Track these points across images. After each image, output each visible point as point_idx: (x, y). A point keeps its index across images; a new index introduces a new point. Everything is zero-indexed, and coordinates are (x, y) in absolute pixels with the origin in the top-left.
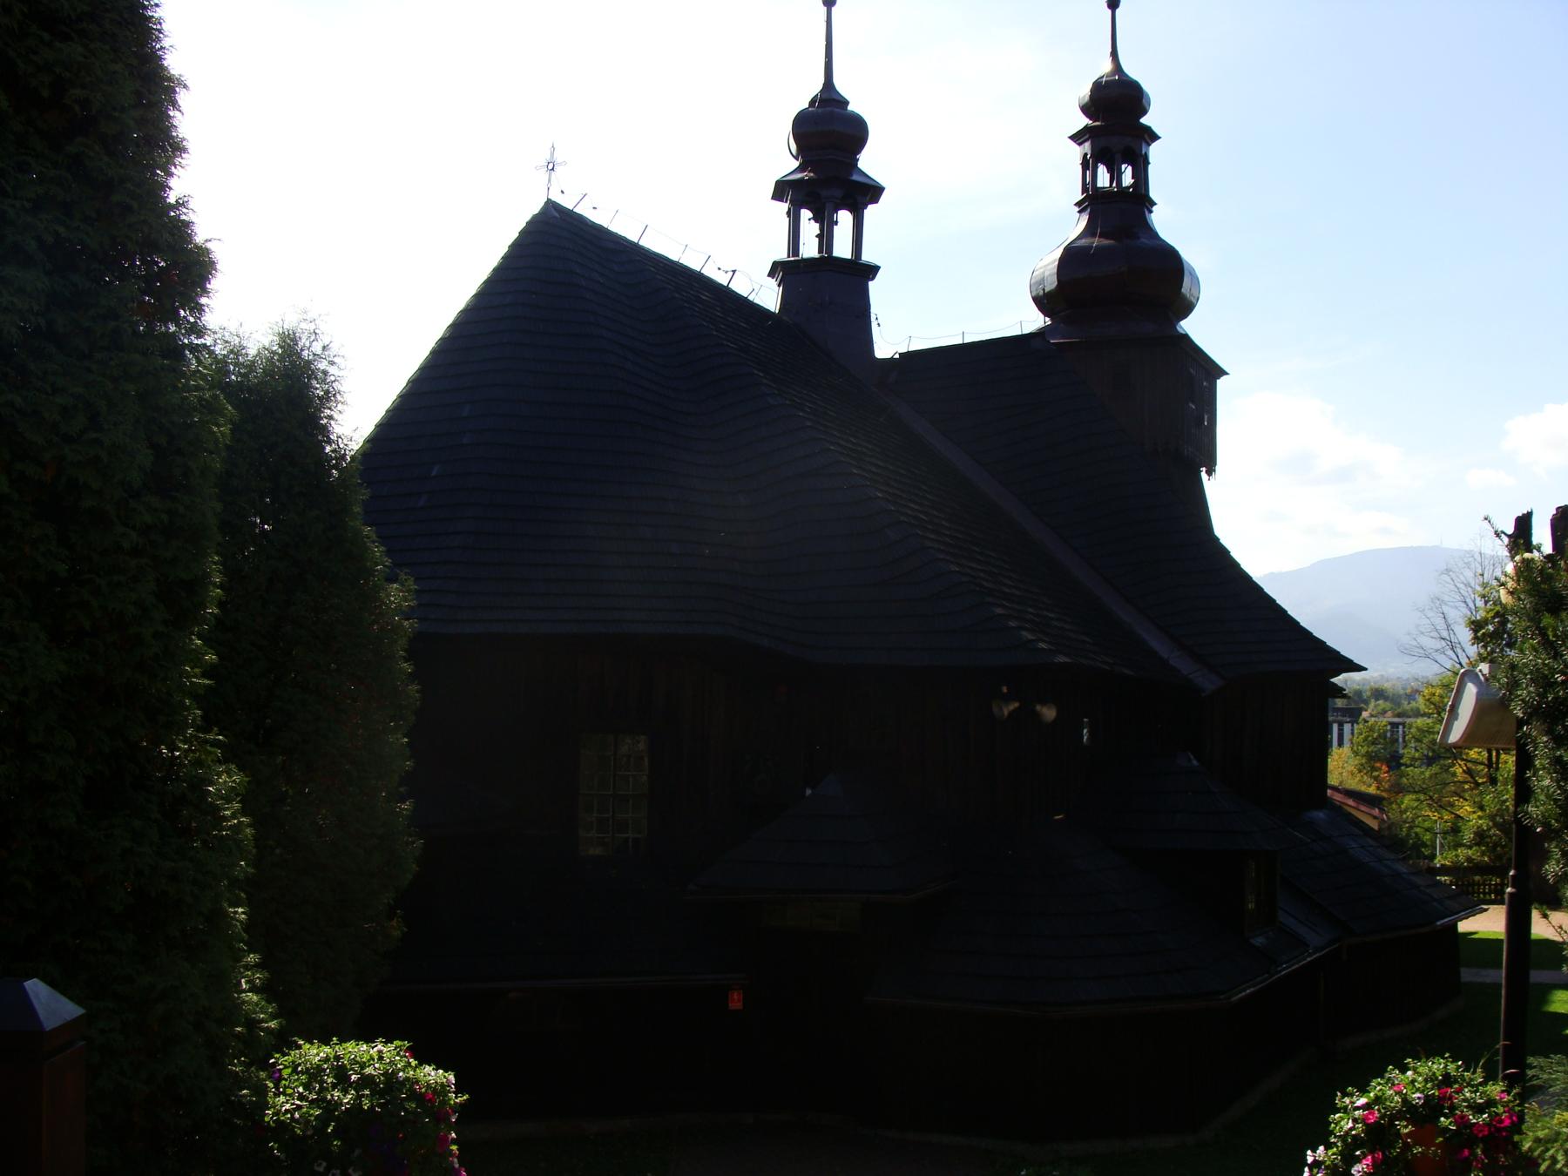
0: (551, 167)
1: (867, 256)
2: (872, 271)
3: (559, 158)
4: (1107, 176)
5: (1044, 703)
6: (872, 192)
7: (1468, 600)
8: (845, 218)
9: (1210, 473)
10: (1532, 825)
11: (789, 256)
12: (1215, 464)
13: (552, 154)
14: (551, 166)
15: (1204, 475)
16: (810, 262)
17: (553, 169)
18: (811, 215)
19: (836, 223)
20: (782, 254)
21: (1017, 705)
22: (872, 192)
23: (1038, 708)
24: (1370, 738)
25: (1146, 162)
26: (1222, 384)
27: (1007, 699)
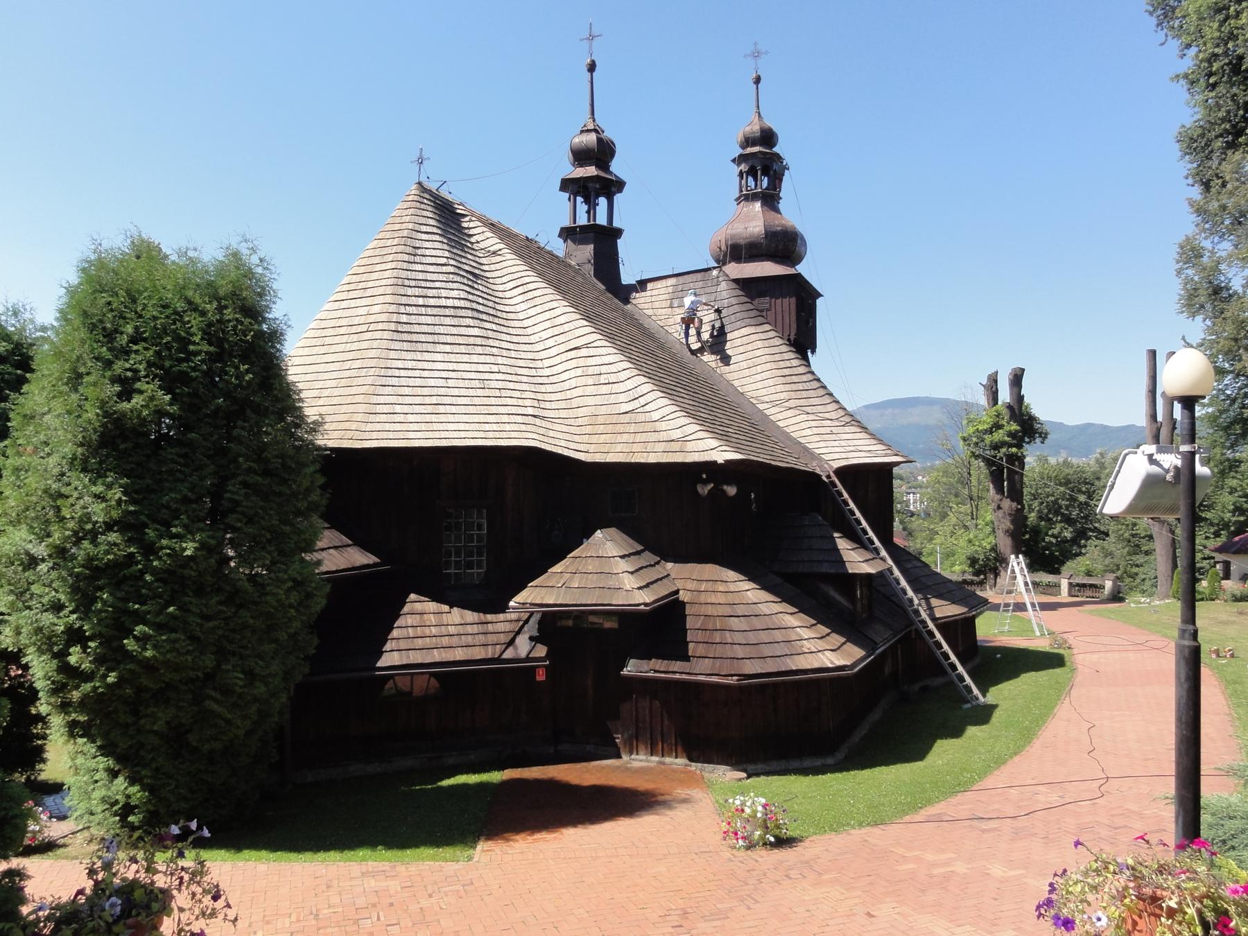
1: (616, 224)
3: (425, 155)
4: (753, 183)
5: (729, 484)
6: (619, 185)
7: (958, 423)
8: (603, 201)
10: (78, 707)
13: (421, 153)
14: (420, 161)
16: (582, 227)
17: (421, 163)
18: (582, 200)
19: (598, 204)
20: (567, 222)
21: (712, 485)
22: (619, 185)
23: (725, 487)
24: (982, 476)
26: (820, 302)
27: (705, 482)
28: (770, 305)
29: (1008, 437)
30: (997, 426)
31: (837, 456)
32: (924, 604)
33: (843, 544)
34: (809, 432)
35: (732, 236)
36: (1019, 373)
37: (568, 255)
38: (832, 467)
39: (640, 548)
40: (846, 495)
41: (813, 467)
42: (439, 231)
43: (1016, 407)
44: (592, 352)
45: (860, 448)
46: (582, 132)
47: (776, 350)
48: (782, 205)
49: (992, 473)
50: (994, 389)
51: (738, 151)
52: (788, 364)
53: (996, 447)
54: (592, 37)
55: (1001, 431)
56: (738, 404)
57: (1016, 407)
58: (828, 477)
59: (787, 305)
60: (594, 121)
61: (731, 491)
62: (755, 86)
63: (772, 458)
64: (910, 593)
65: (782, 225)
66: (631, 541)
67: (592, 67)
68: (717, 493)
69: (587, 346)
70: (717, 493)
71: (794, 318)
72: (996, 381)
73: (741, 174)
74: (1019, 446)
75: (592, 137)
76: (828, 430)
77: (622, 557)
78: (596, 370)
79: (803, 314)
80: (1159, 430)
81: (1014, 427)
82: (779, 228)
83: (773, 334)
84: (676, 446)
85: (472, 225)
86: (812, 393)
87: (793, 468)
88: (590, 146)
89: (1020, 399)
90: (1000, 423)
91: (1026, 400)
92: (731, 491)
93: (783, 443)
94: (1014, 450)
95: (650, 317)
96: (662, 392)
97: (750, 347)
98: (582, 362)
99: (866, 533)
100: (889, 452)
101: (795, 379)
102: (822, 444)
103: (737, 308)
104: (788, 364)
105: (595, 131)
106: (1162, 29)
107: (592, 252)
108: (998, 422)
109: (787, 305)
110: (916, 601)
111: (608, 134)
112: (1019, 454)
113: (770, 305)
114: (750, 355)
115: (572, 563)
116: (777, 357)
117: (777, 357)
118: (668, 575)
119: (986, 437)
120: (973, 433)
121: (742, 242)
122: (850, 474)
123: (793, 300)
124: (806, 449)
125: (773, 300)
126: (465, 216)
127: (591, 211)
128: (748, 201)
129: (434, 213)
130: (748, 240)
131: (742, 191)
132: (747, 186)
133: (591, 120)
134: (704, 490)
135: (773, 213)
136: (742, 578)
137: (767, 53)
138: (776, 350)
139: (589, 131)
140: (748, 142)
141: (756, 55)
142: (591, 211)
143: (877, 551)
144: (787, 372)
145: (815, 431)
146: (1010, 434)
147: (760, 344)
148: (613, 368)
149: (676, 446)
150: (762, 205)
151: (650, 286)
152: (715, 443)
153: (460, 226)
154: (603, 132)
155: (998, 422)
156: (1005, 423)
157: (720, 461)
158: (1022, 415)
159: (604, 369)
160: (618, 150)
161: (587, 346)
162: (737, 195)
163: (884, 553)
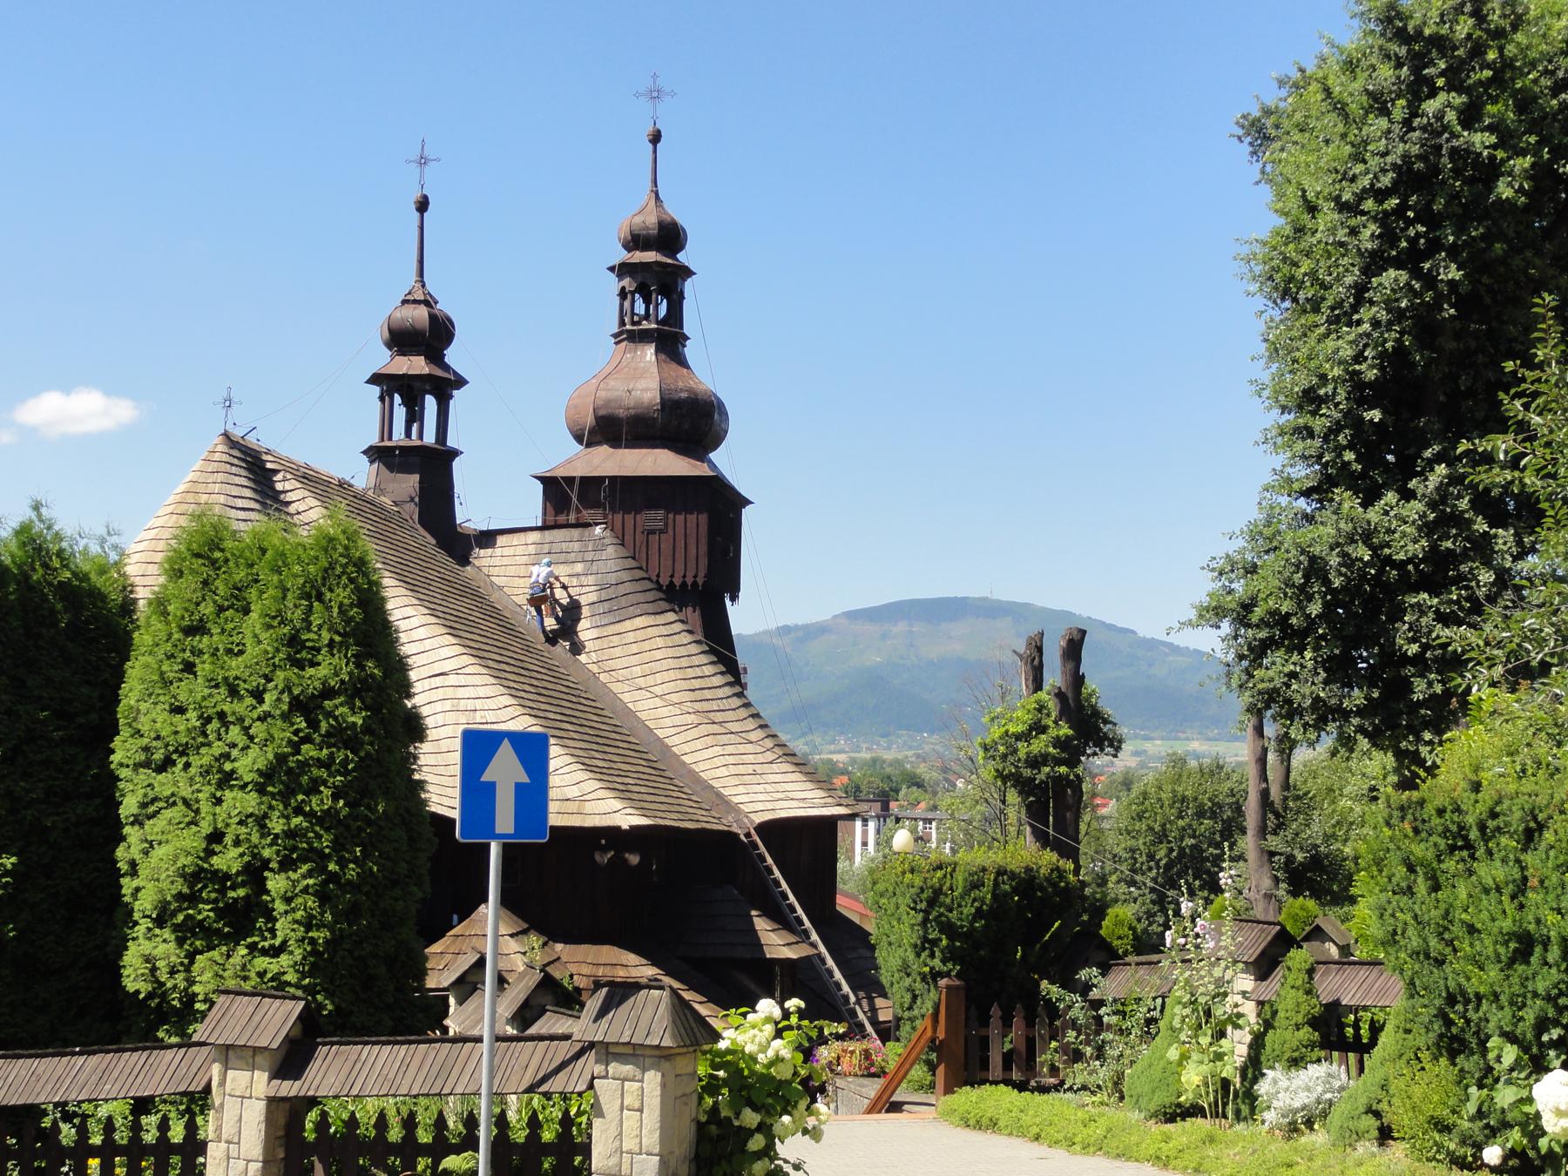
0: (228, 403)
1: (451, 442)
2: (454, 453)
5: (631, 851)
9: (734, 598)
11: (383, 440)
12: (738, 590)
14: (227, 403)
15: (728, 602)
20: (373, 439)
25: (681, 296)
26: (746, 513)
27: (604, 849)
28: (666, 525)
29: (1055, 748)
30: (1038, 728)
31: (760, 806)
32: (865, 1003)
33: (761, 924)
34: (724, 771)
35: (608, 402)
36: (1076, 637)
37: (379, 489)
38: (752, 821)
39: (526, 926)
40: (770, 860)
41: (726, 823)
42: (257, 506)
43: (1070, 695)
44: (462, 680)
45: (791, 795)
46: (404, 302)
47: (682, 651)
48: (690, 351)
49: (1029, 807)
50: (1036, 662)
51: (621, 255)
52: (698, 672)
53: (1035, 762)
54: (423, 161)
55: (1043, 737)
56: (630, 729)
57: (1070, 695)
58: (748, 835)
59: (693, 524)
60: (423, 286)
61: (634, 859)
62: (650, 146)
63: (680, 816)
64: (846, 988)
65: (690, 390)
66: (520, 921)
67: (423, 205)
68: (618, 862)
69: (456, 672)
70: (618, 862)
71: (703, 548)
72: (1040, 649)
73: (623, 294)
74: (1073, 762)
75: (422, 313)
76: (750, 769)
77: (512, 936)
78: (470, 704)
79: (719, 539)
80: (1265, 750)
81: (1065, 730)
82: (684, 395)
83: (678, 627)
84: (572, 807)
85: (288, 486)
86: (730, 715)
87: (703, 830)
88: (418, 326)
89: (1078, 680)
90: (1043, 723)
91: (1091, 684)
92: (634, 859)
93: (690, 788)
94: (1063, 769)
95: (501, 588)
96: (535, 716)
97: (646, 646)
98: (450, 692)
99: (793, 910)
100: (830, 800)
101: (707, 694)
102: (741, 789)
103: (628, 587)
104: (698, 672)
105: (426, 303)
106: (1257, 161)
107: (417, 486)
108: (1040, 720)
109: (693, 524)
110: (853, 999)
111: (445, 306)
112: (1072, 777)
113: (666, 525)
114: (646, 657)
115: (453, 942)
116: (684, 662)
117: (684, 662)
118: (559, 958)
119: (1020, 745)
120: (1001, 738)
121: (621, 413)
122: (776, 831)
123: (704, 518)
124: (719, 795)
125: (671, 516)
126: (276, 472)
127: (414, 416)
128: (634, 342)
129: (249, 479)
130: (632, 412)
131: (624, 325)
132: (633, 314)
133: (419, 285)
134: (604, 858)
135: (674, 366)
136: (644, 961)
137: (673, 94)
138: (682, 651)
139: (415, 302)
140: (636, 241)
141: (655, 95)
142: (414, 416)
143: (806, 934)
144: (697, 684)
145: (733, 770)
146: (1058, 742)
147: (660, 642)
148: (491, 704)
149: (572, 807)
150: (657, 351)
151: (501, 540)
152: (617, 804)
153: (274, 489)
154: (436, 303)
155: (1040, 720)
156: (1051, 723)
157: (625, 826)
158: (1080, 707)
159: (478, 704)
160: (457, 332)
161: (456, 672)
162: (616, 330)
163: (815, 937)
